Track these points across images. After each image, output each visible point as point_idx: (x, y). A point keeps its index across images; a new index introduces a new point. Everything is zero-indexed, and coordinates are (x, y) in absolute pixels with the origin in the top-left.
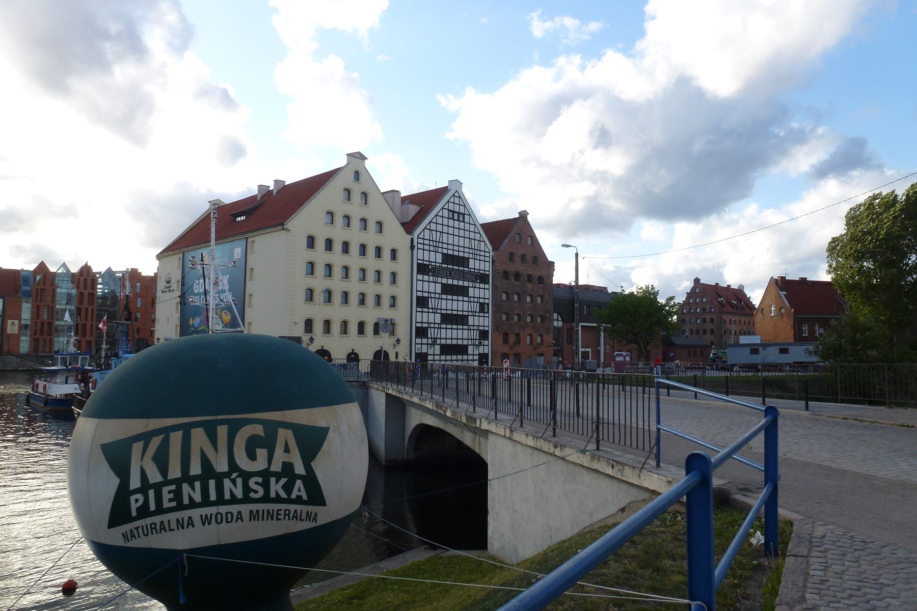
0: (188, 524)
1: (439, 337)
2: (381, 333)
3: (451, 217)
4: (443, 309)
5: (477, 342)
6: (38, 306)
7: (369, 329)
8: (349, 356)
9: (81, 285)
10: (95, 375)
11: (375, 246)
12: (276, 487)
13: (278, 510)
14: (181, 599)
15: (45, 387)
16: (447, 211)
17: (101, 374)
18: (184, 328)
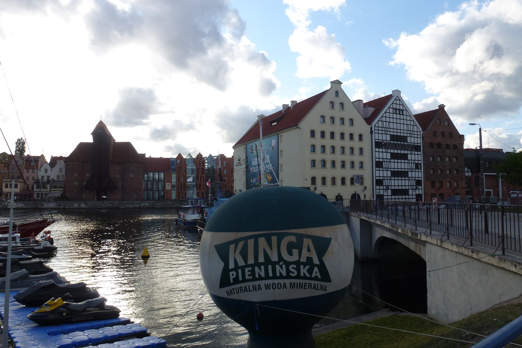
0: (259, 289)
1: (390, 185)
2: (355, 183)
3: (395, 112)
4: (392, 168)
5: (415, 187)
6: (179, 176)
7: (348, 181)
8: (337, 197)
9: (198, 165)
10: (207, 210)
12: (304, 271)
13: (305, 283)
14: (256, 327)
15: (184, 216)
16: (392, 109)
18: (249, 185)
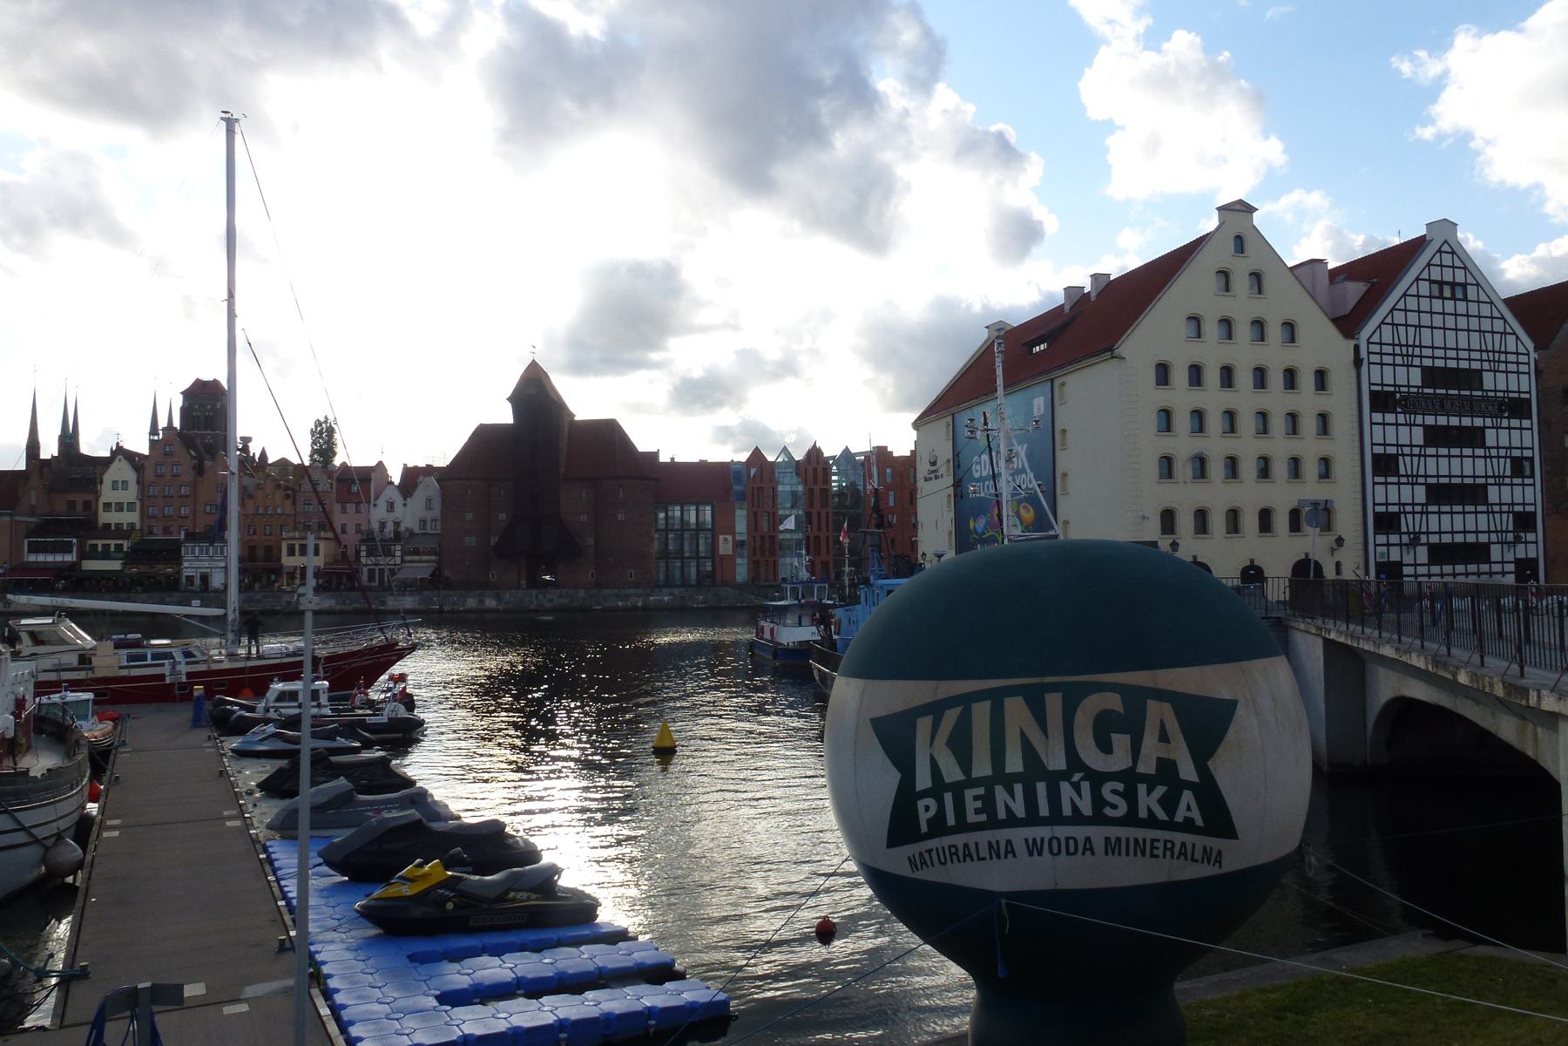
0: (1007, 852)
6: (755, 513)
7: (1281, 521)
10: (839, 613)
11: (1253, 366)
12: (1148, 801)
13: (1153, 841)
15: (772, 631)
17: (847, 610)
18: (963, 539)
